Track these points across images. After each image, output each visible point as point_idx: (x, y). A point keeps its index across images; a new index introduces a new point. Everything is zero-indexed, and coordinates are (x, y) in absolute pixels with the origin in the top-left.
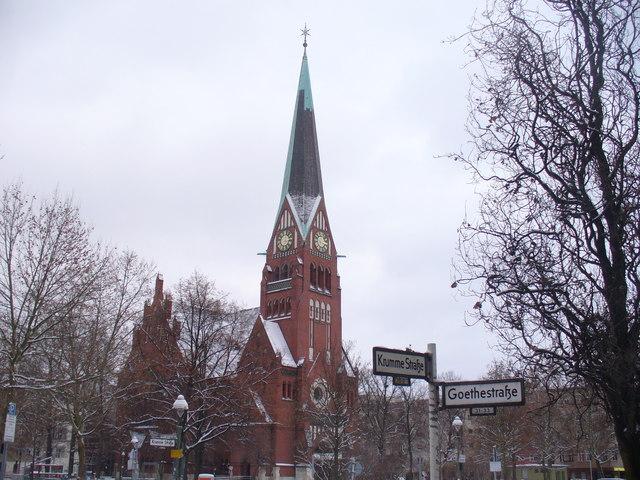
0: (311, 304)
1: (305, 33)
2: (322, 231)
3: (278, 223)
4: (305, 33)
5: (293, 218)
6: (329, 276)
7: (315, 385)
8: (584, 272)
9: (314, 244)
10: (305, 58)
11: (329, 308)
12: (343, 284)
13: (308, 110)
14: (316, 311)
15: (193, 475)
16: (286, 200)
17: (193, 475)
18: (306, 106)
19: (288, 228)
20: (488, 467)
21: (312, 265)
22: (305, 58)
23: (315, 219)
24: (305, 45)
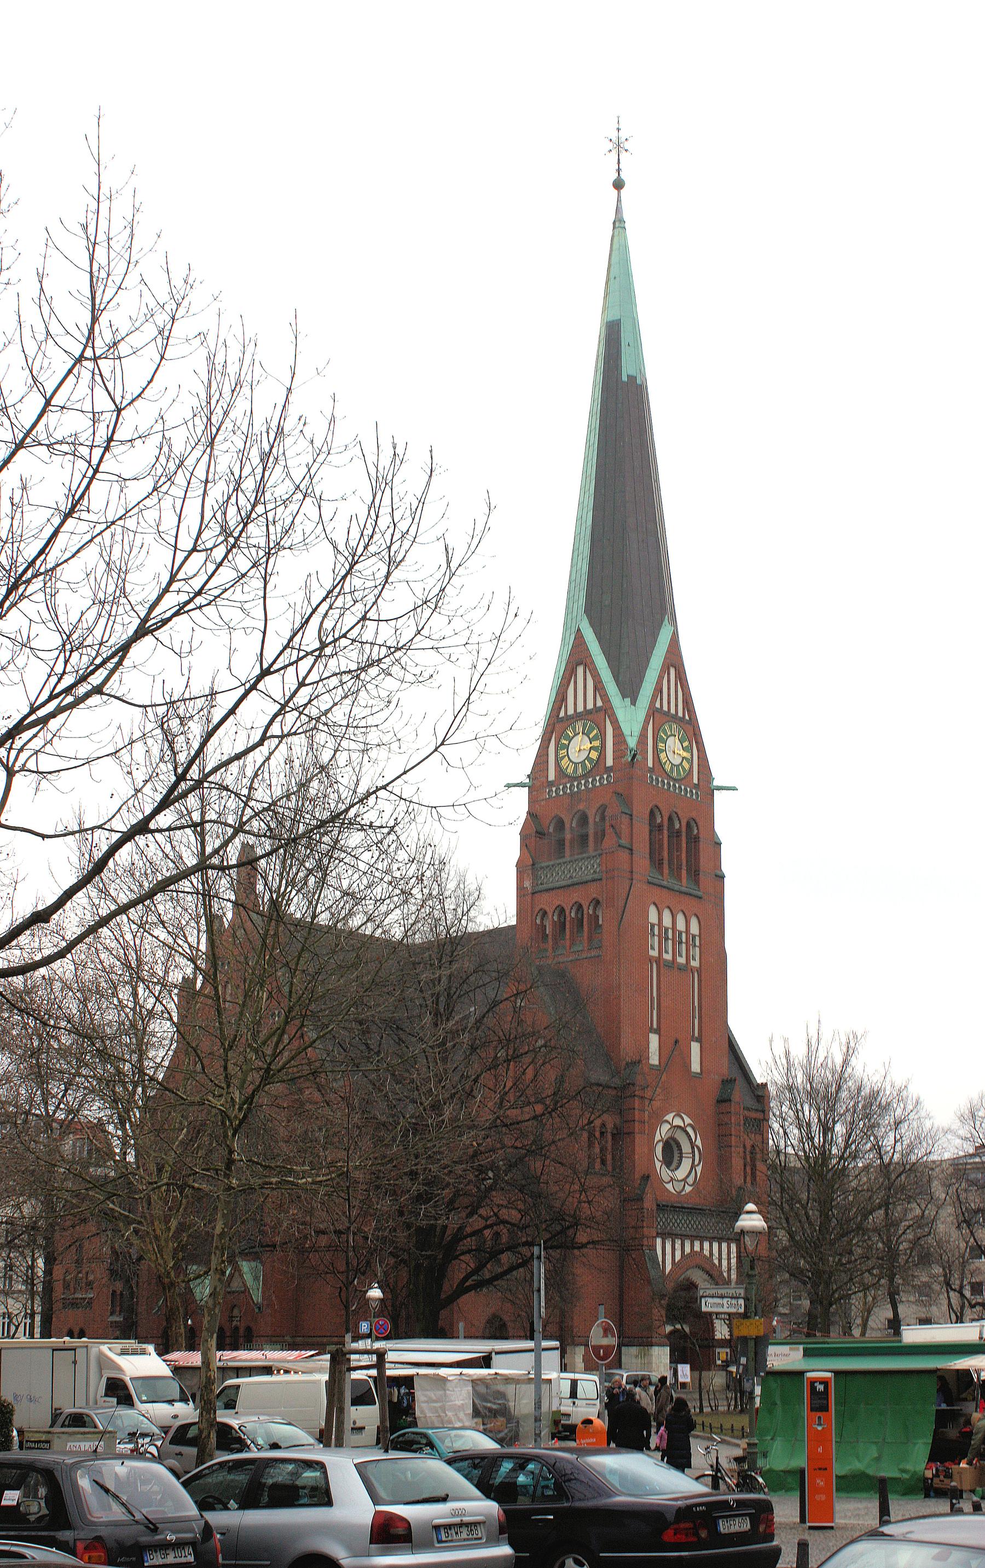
0: (653, 917)
1: (619, 146)
2: (675, 718)
3: (560, 699)
4: (619, 146)
5: (599, 687)
6: (694, 840)
7: (663, 1131)
8: (135, 994)
9: (656, 752)
10: (619, 223)
11: (695, 929)
12: (727, 866)
13: (632, 378)
14: (663, 938)
15: (681, 1380)
16: (579, 635)
17: (681, 1380)
18: (627, 369)
19: (587, 712)
20: (366, 1320)
21: (652, 814)
22: (619, 223)
23: (658, 690)
24: (618, 185)
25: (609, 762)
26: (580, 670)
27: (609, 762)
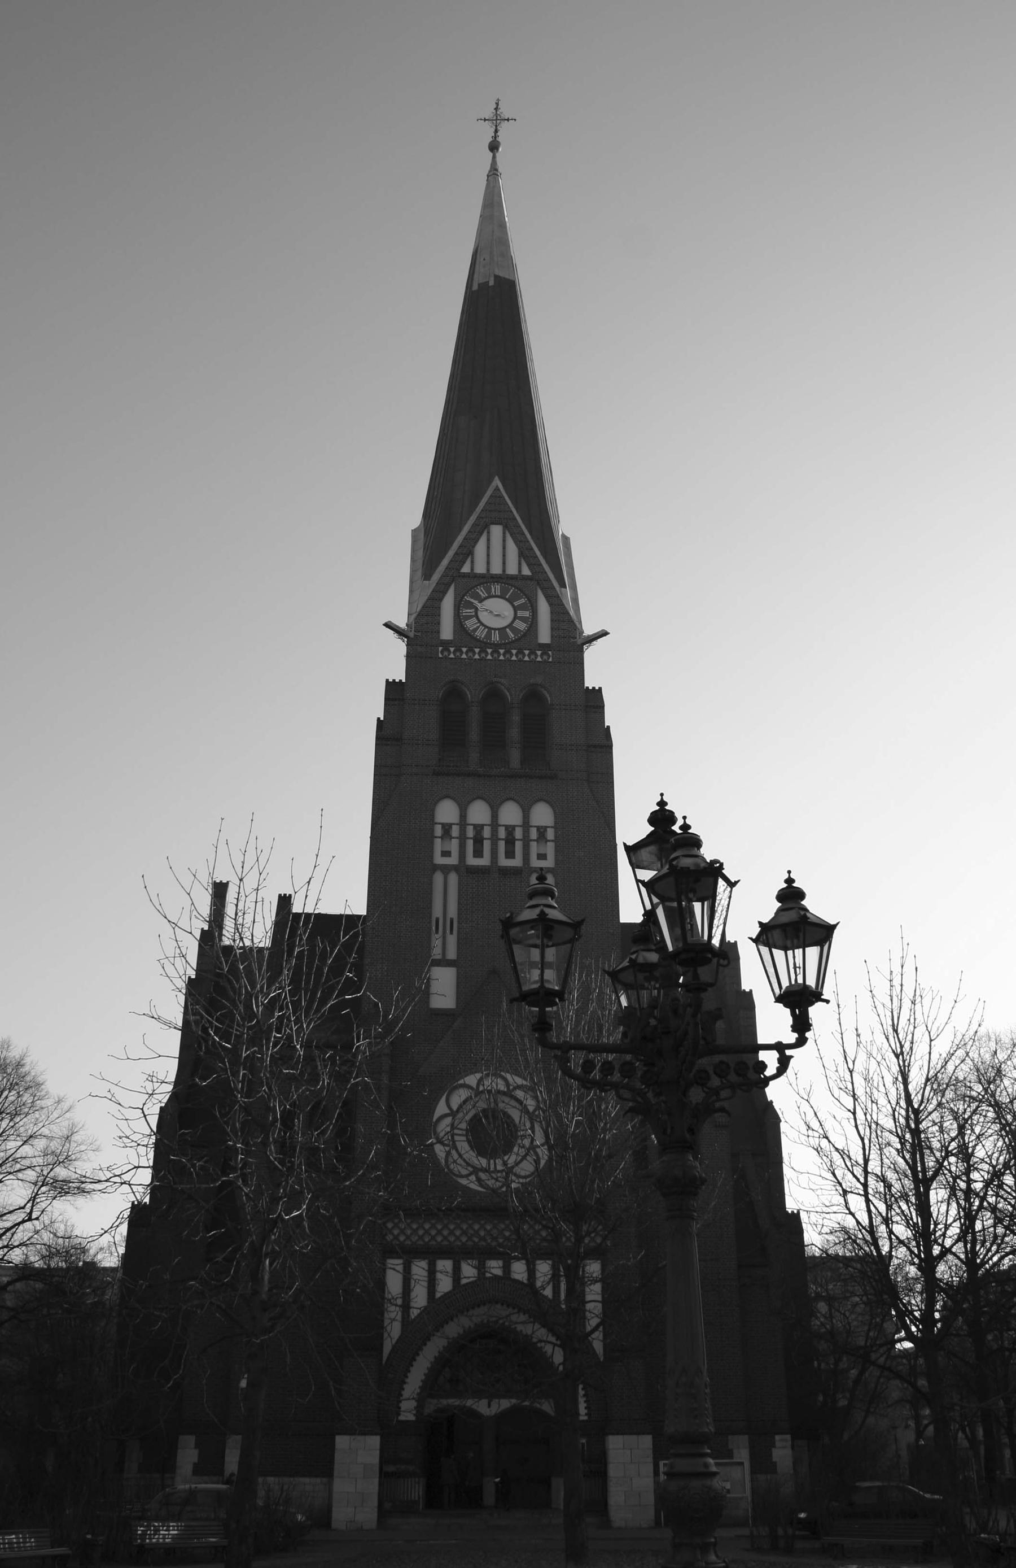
10: (494, 172)
22: (494, 172)
25: (544, 636)
26: (496, 531)
27: (544, 636)
